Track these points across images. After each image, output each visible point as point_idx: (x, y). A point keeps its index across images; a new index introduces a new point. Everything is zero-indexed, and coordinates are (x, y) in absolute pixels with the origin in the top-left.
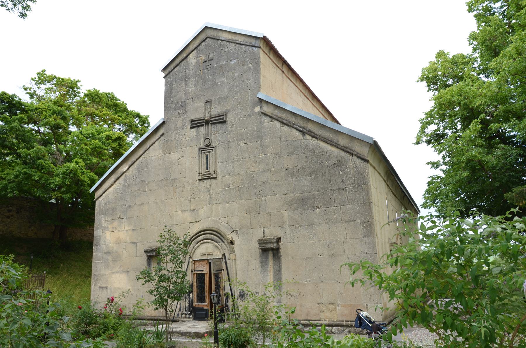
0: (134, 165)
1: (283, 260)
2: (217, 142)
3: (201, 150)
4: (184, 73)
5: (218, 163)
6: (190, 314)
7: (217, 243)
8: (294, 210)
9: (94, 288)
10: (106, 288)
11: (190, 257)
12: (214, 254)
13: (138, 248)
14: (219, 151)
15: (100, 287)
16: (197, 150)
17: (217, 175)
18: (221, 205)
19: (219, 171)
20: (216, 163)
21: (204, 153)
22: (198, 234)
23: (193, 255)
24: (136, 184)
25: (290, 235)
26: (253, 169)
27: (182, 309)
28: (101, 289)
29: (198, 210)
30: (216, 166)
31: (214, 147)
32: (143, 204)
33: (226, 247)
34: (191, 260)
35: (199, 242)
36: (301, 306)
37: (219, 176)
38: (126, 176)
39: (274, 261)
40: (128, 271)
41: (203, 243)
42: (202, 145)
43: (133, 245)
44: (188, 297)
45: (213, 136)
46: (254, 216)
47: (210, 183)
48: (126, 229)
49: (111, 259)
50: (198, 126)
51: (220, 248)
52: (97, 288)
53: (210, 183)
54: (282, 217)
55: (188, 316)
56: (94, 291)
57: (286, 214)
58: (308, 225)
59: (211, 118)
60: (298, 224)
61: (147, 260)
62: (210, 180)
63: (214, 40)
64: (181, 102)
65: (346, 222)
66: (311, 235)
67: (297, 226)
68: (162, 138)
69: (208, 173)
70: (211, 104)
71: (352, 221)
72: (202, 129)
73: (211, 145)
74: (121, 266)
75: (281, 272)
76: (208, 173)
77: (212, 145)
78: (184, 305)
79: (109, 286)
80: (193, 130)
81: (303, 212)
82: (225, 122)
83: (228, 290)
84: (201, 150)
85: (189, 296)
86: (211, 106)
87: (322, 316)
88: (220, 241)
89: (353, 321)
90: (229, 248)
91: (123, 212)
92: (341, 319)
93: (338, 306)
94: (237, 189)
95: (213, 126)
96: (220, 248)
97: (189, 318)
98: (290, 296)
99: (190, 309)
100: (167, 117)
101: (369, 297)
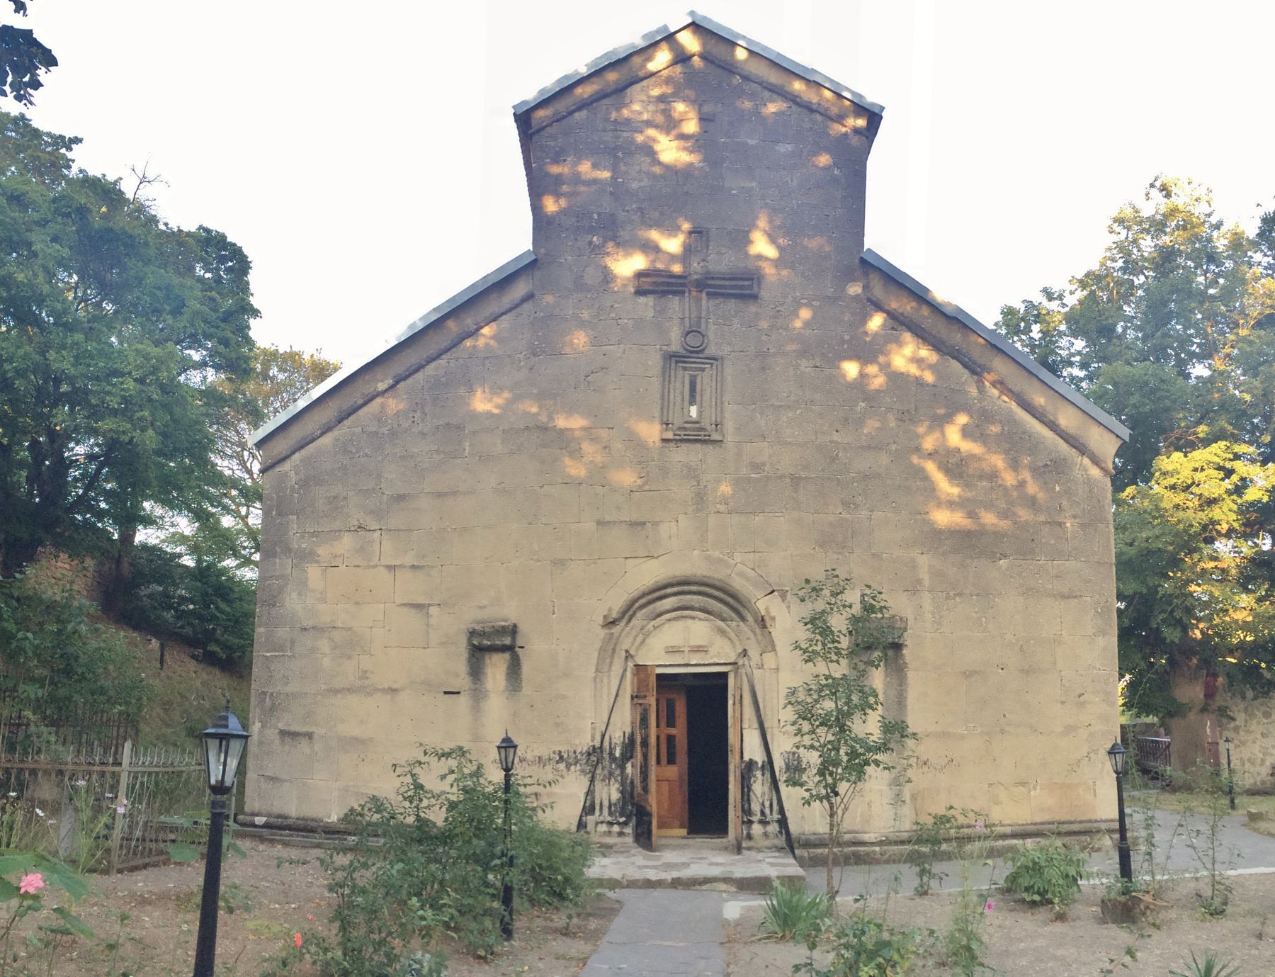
0: (416, 376)
1: (911, 675)
2: (727, 349)
3: (673, 359)
4: (610, 134)
5: (726, 404)
6: (625, 824)
7: (723, 620)
8: (944, 554)
9: (260, 732)
10: (310, 736)
11: (628, 656)
12: (713, 651)
13: (433, 621)
14: (729, 371)
15: (283, 733)
16: (655, 361)
17: (724, 435)
18: (736, 519)
19: (729, 426)
20: (722, 403)
21: (685, 369)
22: (657, 592)
23: (637, 649)
24: (423, 434)
25: (933, 614)
26: (836, 437)
27: (597, 808)
28: (288, 739)
29: (656, 524)
30: (722, 412)
31: (716, 359)
32: (454, 493)
33: (751, 635)
34: (630, 664)
35: (660, 615)
36: (949, 792)
37: (730, 437)
38: (383, 406)
39: (886, 676)
40: (395, 691)
41: (674, 619)
42: (675, 347)
43: (413, 611)
44: (618, 772)
45: (713, 328)
46: (836, 556)
47: (700, 456)
48: (384, 562)
49: (327, 650)
50: (664, 293)
51: (732, 635)
52: (272, 734)
53: (700, 456)
54: (915, 567)
55: (616, 828)
56: (261, 743)
57: (924, 561)
58: (978, 595)
59: (707, 278)
60: (954, 589)
61: (469, 660)
62: (698, 446)
63: (719, 71)
64: (599, 214)
65: (1064, 597)
66: (984, 619)
67: (951, 594)
68: (527, 307)
69: (697, 425)
70: (708, 240)
71: (1075, 597)
72: (677, 302)
73: (706, 351)
74: (667, 424)
75: (905, 706)
76: (697, 425)
77: (708, 352)
78: (605, 797)
79: (319, 731)
80: (642, 300)
81: (969, 561)
82: (755, 297)
83: (753, 750)
84: (673, 359)
85: (623, 768)
86: (708, 246)
87: (996, 815)
88: (734, 615)
89: (1112, 821)
90: (760, 637)
91: (372, 512)
92: (1038, 820)
93: (1035, 788)
94: (788, 480)
95: (713, 303)
96: (732, 635)
97: (621, 834)
98: (925, 768)
99: (623, 808)
100: (543, 251)
101: (1100, 765)
